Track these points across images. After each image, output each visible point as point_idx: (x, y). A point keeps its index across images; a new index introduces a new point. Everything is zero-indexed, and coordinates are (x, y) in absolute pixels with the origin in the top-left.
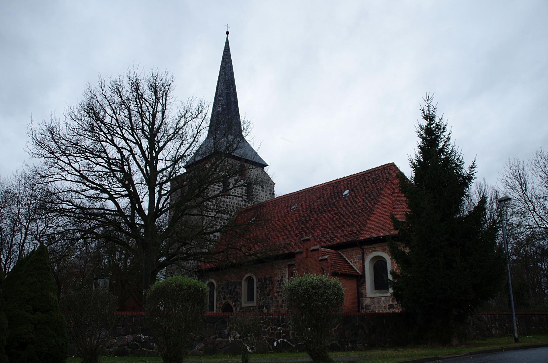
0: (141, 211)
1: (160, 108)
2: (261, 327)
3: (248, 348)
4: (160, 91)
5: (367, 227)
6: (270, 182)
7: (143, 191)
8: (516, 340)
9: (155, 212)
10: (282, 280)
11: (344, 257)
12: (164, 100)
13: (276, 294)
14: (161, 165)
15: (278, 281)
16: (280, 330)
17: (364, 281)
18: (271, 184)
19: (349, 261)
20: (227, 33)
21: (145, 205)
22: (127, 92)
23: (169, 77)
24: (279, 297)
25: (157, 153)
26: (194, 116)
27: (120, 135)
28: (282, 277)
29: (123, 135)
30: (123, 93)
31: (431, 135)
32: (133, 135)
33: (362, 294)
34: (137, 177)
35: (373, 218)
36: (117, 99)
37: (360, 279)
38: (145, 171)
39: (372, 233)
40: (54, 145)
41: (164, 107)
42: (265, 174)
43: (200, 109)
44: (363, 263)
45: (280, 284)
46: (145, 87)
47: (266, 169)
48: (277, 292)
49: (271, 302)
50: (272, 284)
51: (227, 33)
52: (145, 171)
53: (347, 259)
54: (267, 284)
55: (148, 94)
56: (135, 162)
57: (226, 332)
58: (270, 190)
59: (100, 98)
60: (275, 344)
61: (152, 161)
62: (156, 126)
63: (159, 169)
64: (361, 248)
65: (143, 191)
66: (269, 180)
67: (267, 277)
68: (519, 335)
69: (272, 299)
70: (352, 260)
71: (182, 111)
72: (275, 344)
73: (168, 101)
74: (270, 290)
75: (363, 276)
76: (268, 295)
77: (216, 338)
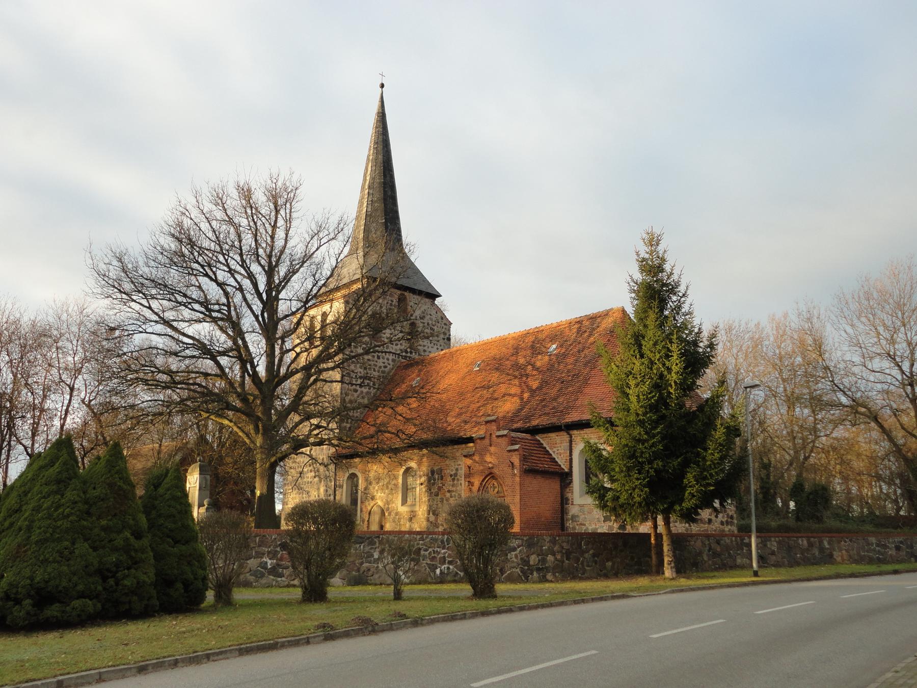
0: (255, 376)
1: (281, 222)
2: (420, 549)
3: (403, 577)
4: (281, 200)
5: (578, 403)
6: (444, 321)
7: (256, 343)
8: (756, 574)
9: (275, 378)
10: (456, 475)
11: (545, 445)
12: (288, 211)
13: (448, 495)
14: (283, 308)
15: (451, 476)
16: (445, 553)
17: (571, 481)
18: (445, 324)
19: (551, 452)
20: (382, 86)
21: (261, 370)
22: (234, 201)
23: (295, 178)
24: (451, 499)
25: (279, 292)
26: (332, 236)
27: (224, 264)
28: (457, 470)
29: (228, 266)
30: (229, 203)
31: (657, 291)
32: (242, 266)
33: (567, 499)
34: (248, 322)
35: (586, 390)
36: (220, 215)
37: (565, 478)
38: (260, 319)
39: (583, 413)
40: (128, 282)
41: (288, 221)
42: (438, 310)
43: (341, 225)
44: (571, 455)
45: (453, 480)
46: (260, 198)
47: (438, 301)
48: (449, 491)
49: (440, 505)
50: (442, 479)
51: (382, 86)
52: (260, 319)
53: (548, 448)
54: (434, 480)
55: (266, 208)
56: (249, 311)
57: (376, 555)
58: (445, 334)
59: (195, 213)
60: (438, 571)
61: (270, 304)
62: (276, 251)
63: (280, 314)
64: (569, 434)
65: (256, 343)
66: (442, 318)
67: (435, 468)
68: (759, 567)
69: (442, 501)
70: (555, 449)
71: (314, 227)
72: (438, 571)
73: (294, 215)
74: (440, 488)
75: (569, 474)
76: (437, 495)
77: (362, 563)
